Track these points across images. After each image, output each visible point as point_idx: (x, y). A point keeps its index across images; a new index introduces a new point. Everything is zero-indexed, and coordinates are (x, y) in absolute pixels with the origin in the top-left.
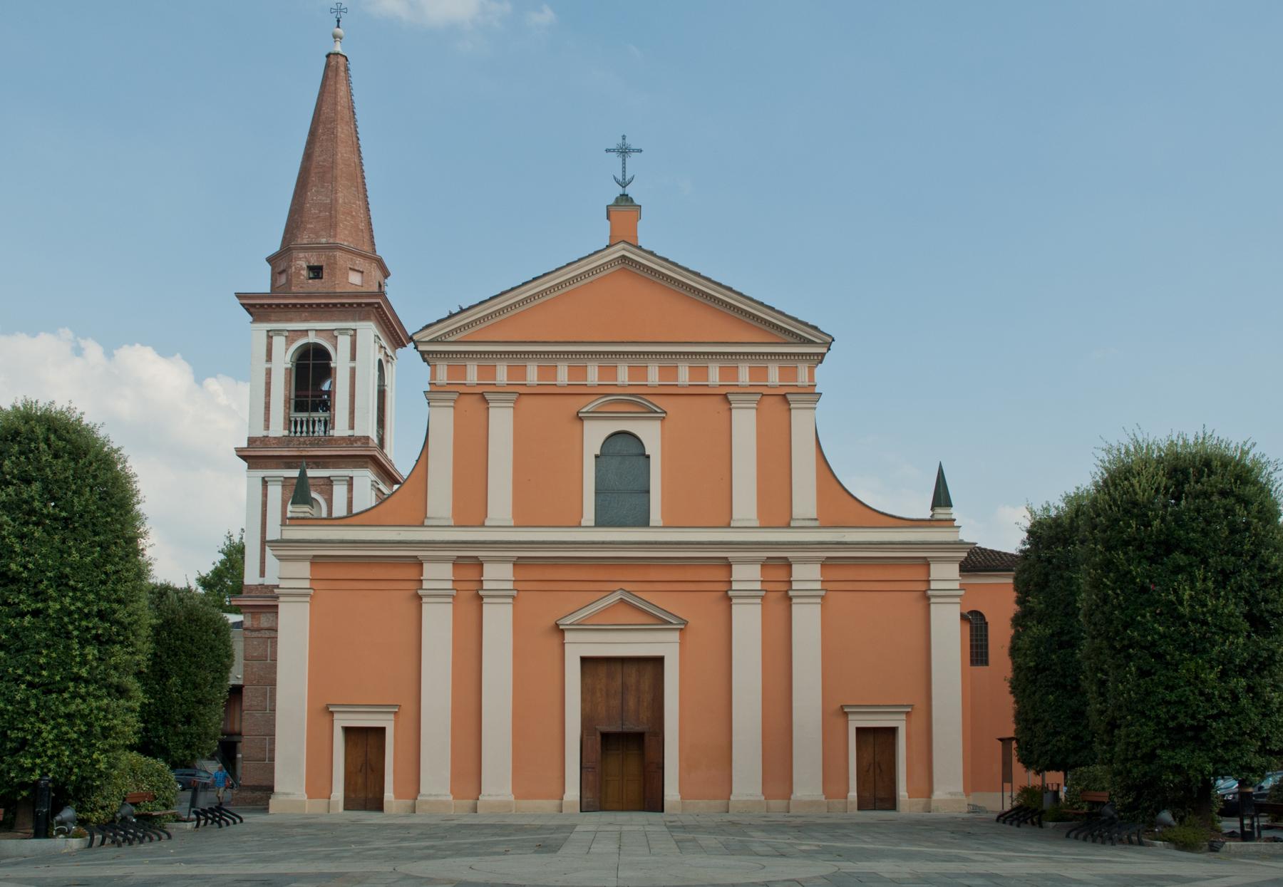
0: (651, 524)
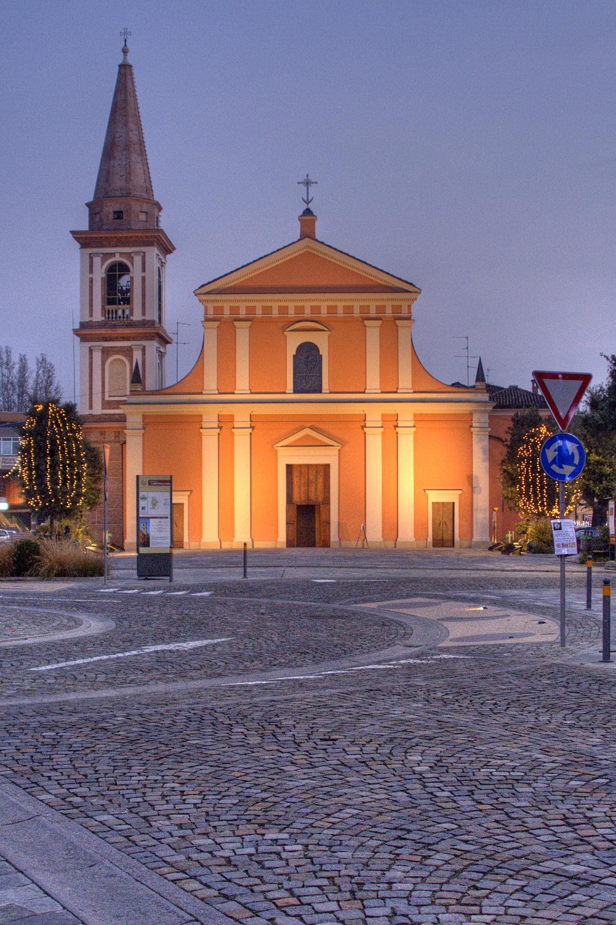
0: (323, 391)
